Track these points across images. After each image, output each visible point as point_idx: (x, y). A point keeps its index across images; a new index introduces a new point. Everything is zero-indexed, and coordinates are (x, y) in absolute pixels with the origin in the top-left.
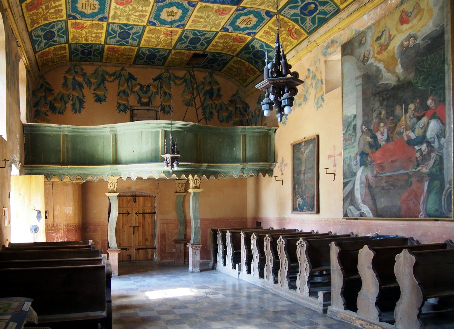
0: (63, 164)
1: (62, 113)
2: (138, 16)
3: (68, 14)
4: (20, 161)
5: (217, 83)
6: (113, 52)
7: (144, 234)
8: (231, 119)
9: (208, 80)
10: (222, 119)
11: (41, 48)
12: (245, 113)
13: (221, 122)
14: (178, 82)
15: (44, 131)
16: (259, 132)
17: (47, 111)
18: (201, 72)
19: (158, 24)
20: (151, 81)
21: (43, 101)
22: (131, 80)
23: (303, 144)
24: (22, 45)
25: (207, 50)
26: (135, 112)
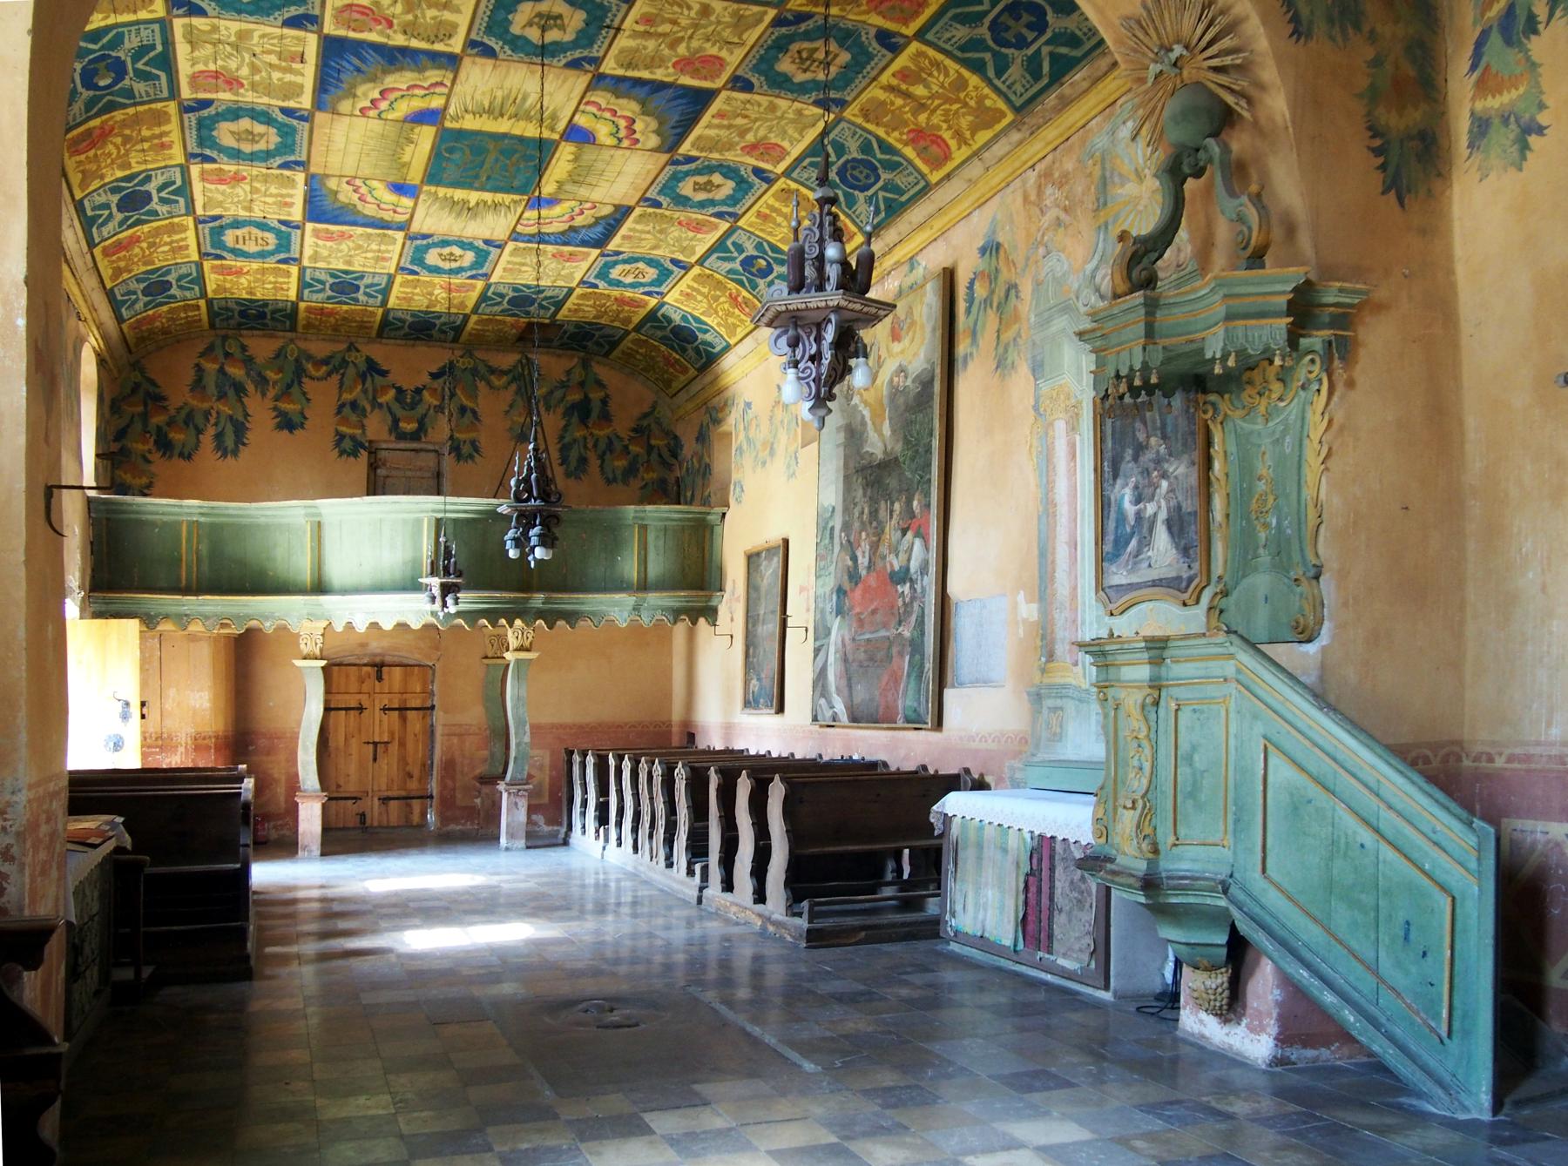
1: (189, 457)
2: (373, 258)
3: (203, 251)
4: (81, 587)
5: (600, 384)
7: (403, 760)
8: (635, 476)
9: (577, 376)
10: (611, 476)
12: (673, 461)
13: (609, 482)
14: (496, 382)
15: (137, 513)
16: (680, 520)
17: (150, 451)
18: (559, 356)
20: (426, 379)
21: (138, 426)
24: (88, 316)
25: (559, 317)
26: (382, 454)
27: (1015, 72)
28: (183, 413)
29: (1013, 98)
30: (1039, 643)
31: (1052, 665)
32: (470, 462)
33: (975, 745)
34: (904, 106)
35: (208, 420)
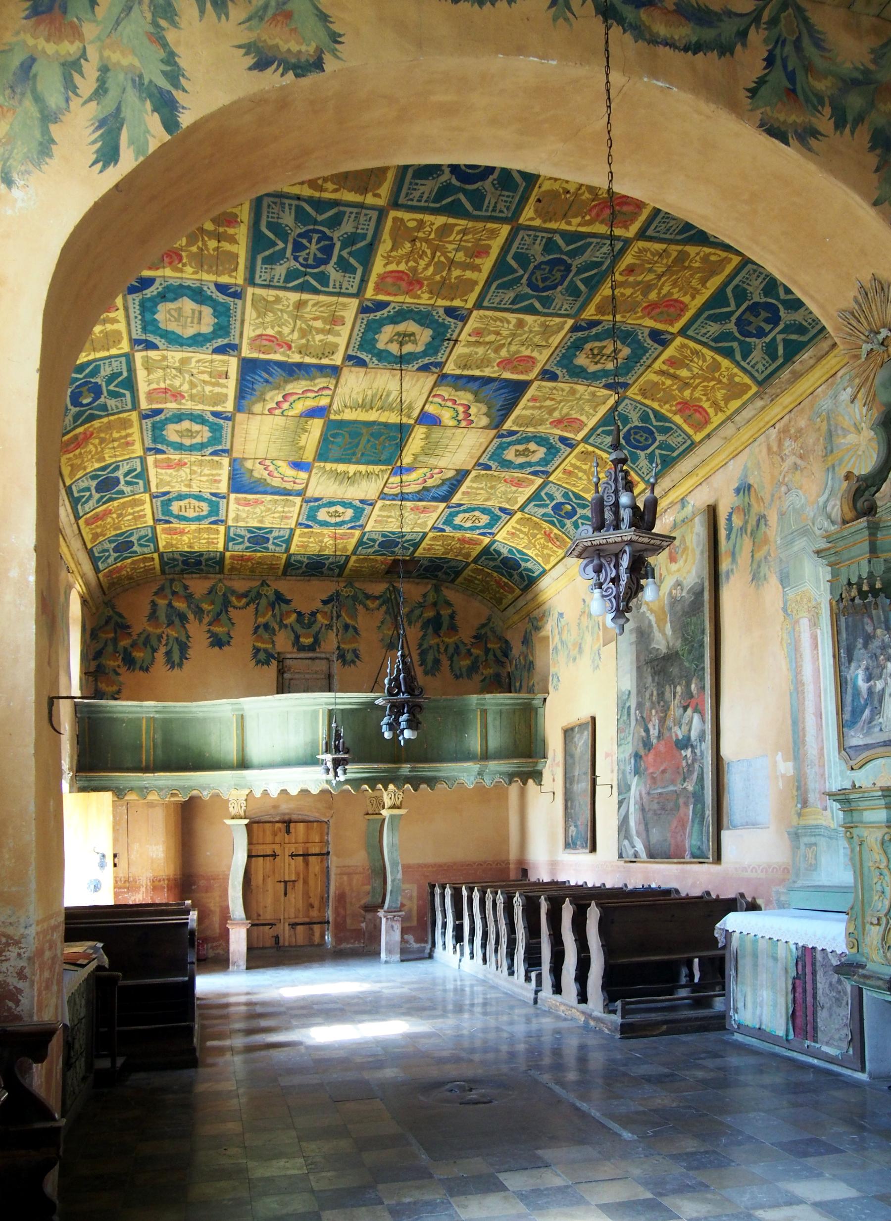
0: (147, 769)
1: (147, 670)
2: (278, 517)
5: (448, 604)
6: (242, 560)
7: (306, 895)
9: (431, 599)
11: (110, 364)
12: (504, 659)
13: (457, 677)
16: (512, 704)
17: (119, 667)
18: (418, 584)
19: (316, 526)
20: (319, 605)
21: (110, 649)
22: (279, 604)
23: (576, 729)
24: (75, 569)
25: (416, 554)
26: (288, 662)
27: (757, 355)
28: (143, 636)
29: (756, 374)
30: (795, 793)
31: (807, 810)
32: (352, 665)
33: (748, 874)
34: (672, 385)
35: (160, 642)
